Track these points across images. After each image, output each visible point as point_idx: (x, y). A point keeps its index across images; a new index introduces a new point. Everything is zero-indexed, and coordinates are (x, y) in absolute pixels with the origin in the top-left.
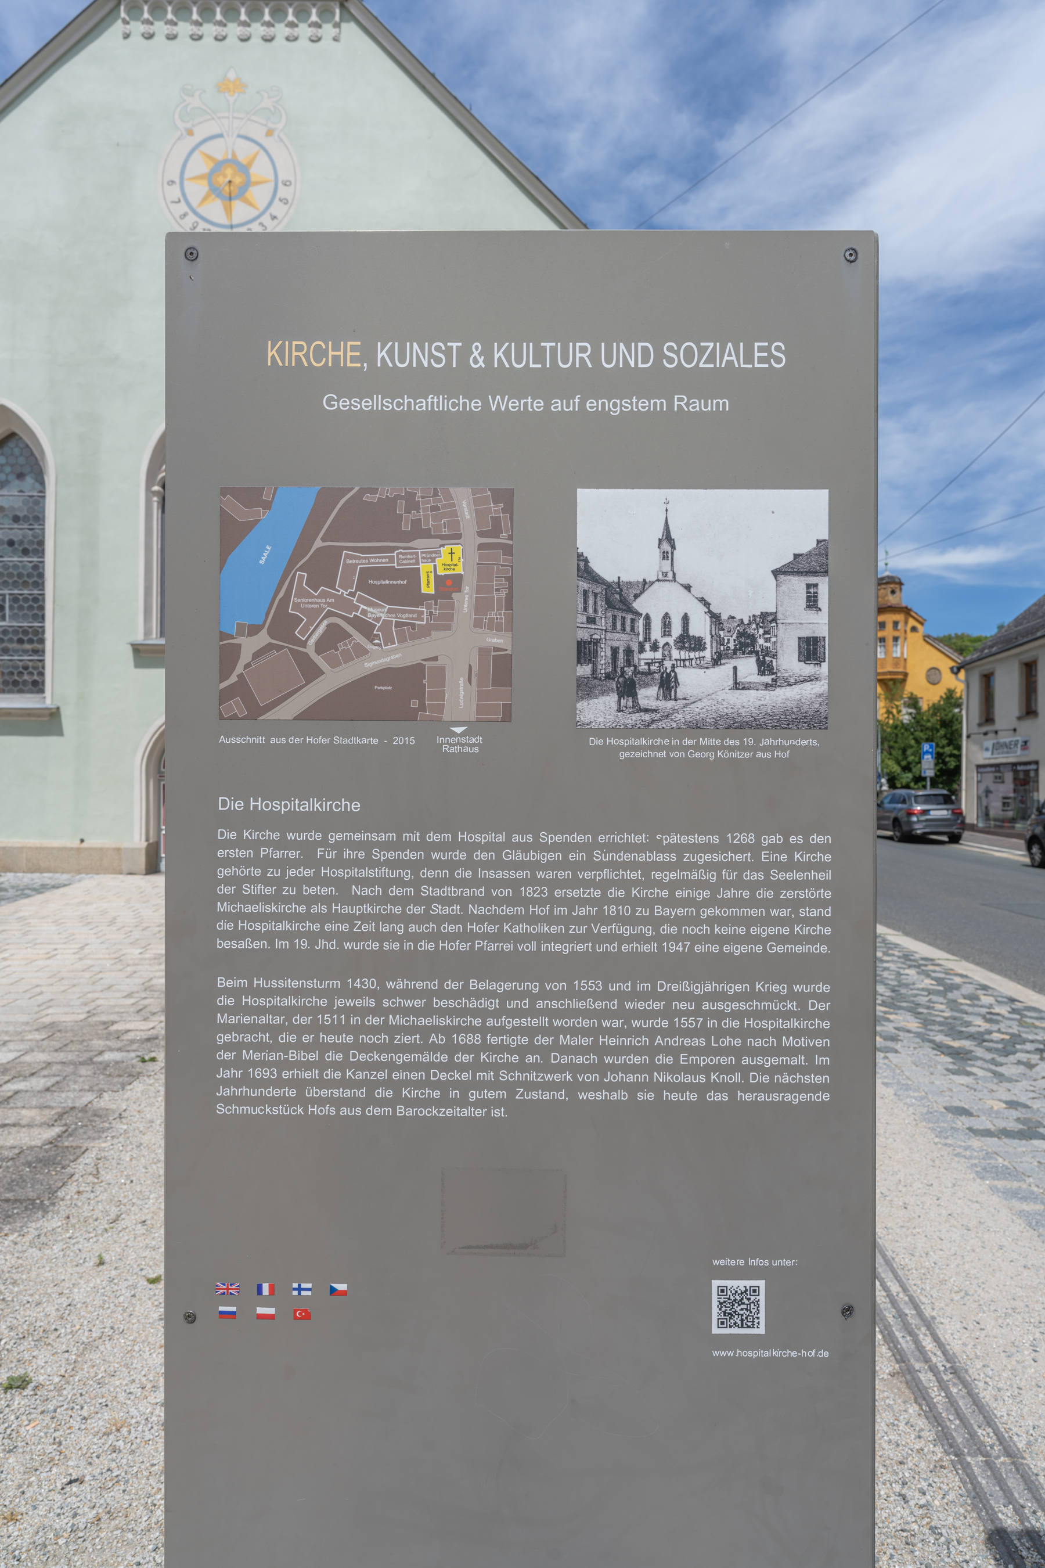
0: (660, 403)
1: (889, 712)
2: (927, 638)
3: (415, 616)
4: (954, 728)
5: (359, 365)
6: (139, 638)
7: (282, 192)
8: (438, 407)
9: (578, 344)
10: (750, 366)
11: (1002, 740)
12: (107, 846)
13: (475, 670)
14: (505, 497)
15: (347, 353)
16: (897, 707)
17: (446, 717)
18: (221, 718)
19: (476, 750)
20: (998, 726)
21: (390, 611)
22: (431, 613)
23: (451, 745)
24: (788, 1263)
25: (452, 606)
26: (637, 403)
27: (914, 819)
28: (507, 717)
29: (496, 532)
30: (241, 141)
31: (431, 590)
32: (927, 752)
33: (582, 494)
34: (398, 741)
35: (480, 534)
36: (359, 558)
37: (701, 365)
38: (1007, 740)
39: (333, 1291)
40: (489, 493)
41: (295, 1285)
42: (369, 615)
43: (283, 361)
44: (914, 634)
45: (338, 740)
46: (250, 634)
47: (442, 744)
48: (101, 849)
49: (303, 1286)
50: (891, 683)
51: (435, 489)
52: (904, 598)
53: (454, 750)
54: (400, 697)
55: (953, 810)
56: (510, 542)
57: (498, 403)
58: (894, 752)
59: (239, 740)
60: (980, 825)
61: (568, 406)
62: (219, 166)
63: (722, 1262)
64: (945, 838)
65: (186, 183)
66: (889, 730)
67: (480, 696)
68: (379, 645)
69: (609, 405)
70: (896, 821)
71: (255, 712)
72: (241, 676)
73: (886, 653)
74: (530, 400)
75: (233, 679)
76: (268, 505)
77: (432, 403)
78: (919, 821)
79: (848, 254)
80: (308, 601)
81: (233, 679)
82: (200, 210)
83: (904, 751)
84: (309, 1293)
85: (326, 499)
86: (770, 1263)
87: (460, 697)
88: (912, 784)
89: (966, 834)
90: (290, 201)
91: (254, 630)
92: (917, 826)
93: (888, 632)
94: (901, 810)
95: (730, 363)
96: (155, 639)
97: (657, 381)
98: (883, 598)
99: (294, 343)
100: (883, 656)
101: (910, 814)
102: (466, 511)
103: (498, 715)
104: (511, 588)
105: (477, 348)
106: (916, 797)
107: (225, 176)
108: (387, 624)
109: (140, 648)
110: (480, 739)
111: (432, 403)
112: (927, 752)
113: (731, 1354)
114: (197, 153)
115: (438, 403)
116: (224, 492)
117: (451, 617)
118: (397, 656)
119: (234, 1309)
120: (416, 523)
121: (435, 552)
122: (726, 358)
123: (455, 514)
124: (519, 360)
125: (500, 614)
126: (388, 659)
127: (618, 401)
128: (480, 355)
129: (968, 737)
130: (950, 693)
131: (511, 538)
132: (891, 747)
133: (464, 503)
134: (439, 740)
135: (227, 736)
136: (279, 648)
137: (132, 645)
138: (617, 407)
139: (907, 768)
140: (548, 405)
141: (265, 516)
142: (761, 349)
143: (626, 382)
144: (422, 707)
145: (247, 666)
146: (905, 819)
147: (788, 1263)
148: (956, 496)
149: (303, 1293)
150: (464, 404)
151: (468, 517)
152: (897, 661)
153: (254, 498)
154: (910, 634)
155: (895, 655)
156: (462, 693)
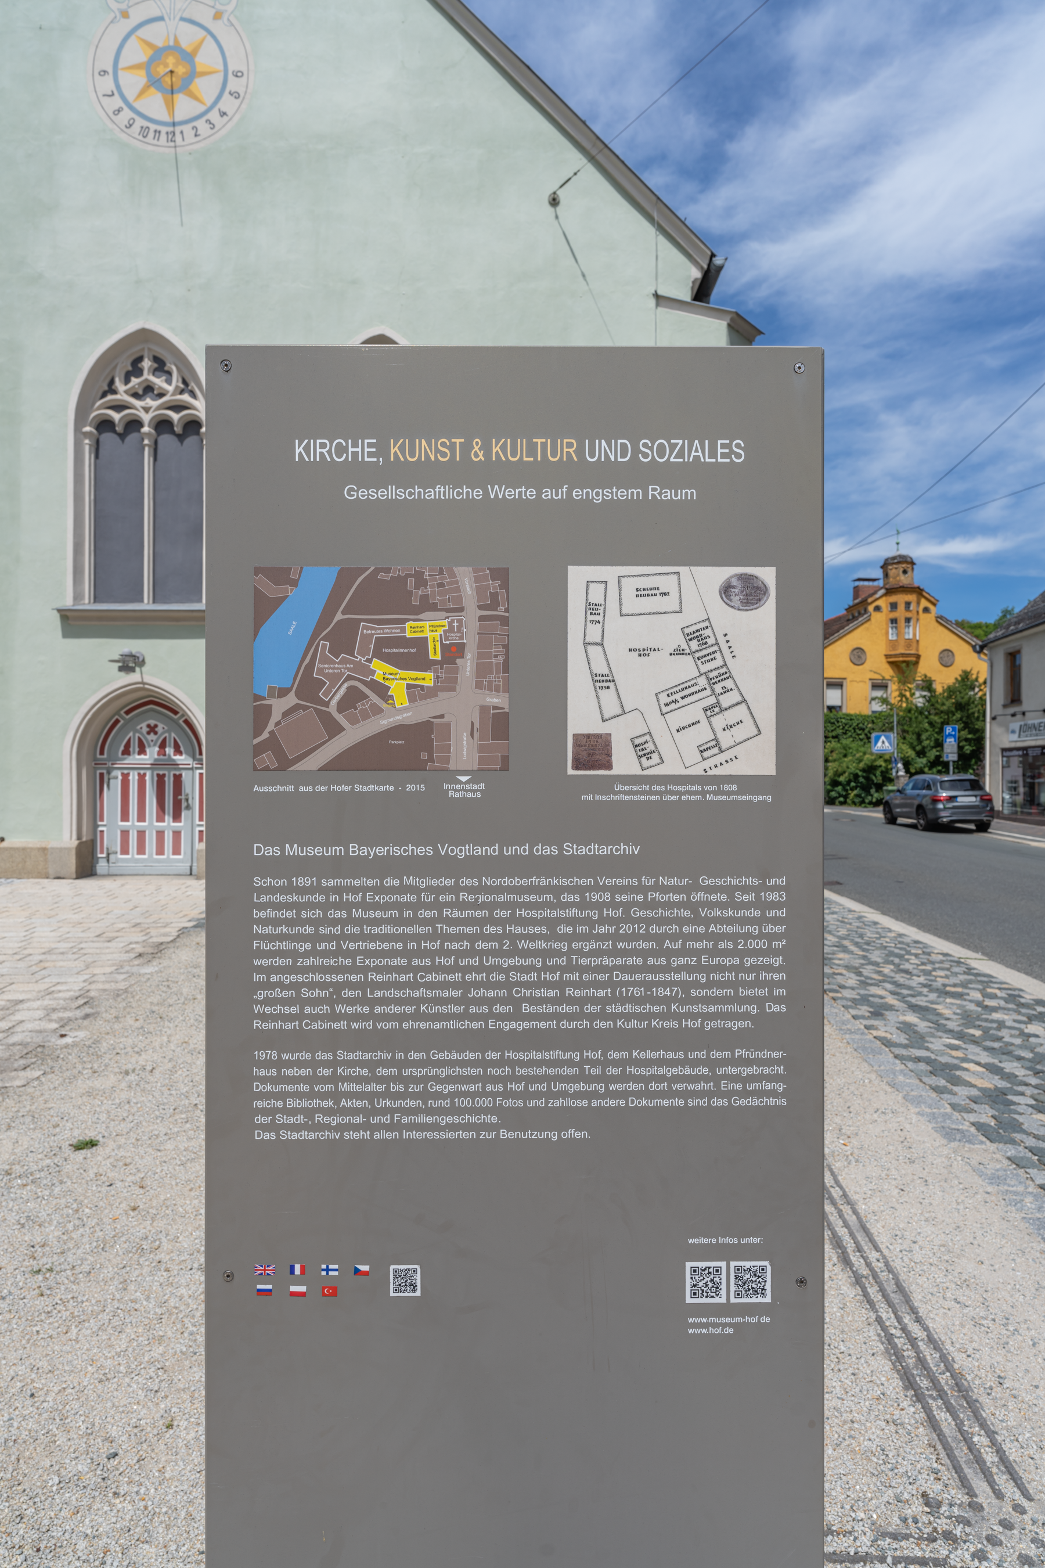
0: (636, 492)
1: (902, 695)
2: (940, 620)
4: (971, 711)
6: (68, 602)
7: (233, 84)
8: (444, 495)
11: (1030, 722)
12: (30, 846)
13: (476, 726)
14: (501, 575)
15: (364, 450)
16: (910, 689)
17: (452, 766)
19: (479, 795)
20: (1025, 706)
22: (438, 677)
23: (456, 791)
27: (940, 806)
28: (505, 767)
29: (494, 605)
30: (184, 25)
31: (438, 657)
32: (950, 735)
33: (569, 567)
34: (410, 788)
35: (480, 607)
36: (375, 629)
37: (672, 460)
38: (1036, 722)
39: (357, 1271)
41: (324, 1267)
43: (309, 458)
44: (926, 615)
45: (358, 788)
47: (448, 790)
48: (24, 849)
49: (331, 1267)
50: (904, 665)
52: (917, 578)
53: (457, 795)
54: (410, 749)
55: (981, 796)
56: (507, 614)
57: (496, 492)
60: (1006, 812)
61: (557, 495)
62: (158, 54)
63: (696, 1241)
64: (972, 827)
65: (120, 73)
66: (901, 714)
67: (482, 749)
69: (592, 494)
70: (920, 808)
71: (284, 764)
72: (272, 733)
73: (897, 635)
74: (523, 489)
75: (265, 735)
80: (331, 667)
81: (265, 735)
82: (137, 105)
83: (919, 735)
84: (336, 1273)
85: (345, 577)
87: (464, 750)
88: (926, 770)
89: (995, 822)
90: (242, 95)
91: (283, 692)
92: (943, 814)
93: (901, 613)
94: (925, 796)
95: (697, 458)
96: (87, 604)
97: (634, 473)
98: (895, 578)
100: (895, 638)
101: (935, 800)
103: (496, 766)
104: (507, 654)
105: (477, 443)
106: (942, 782)
107: (166, 65)
109: (68, 614)
112: (950, 735)
114: (133, 39)
115: (444, 492)
116: (257, 571)
117: (455, 680)
118: (409, 714)
119: (270, 1287)
122: (693, 454)
123: (458, 589)
124: (514, 455)
126: (400, 717)
129: (994, 718)
130: (966, 675)
131: (507, 610)
132: (904, 731)
133: (466, 580)
134: (446, 786)
135: (260, 785)
137: (59, 611)
138: (599, 496)
139: (921, 753)
142: (723, 446)
143: (607, 474)
144: (431, 759)
145: (278, 724)
146: (931, 807)
147: (756, 1240)
148: (957, 487)
149: (331, 1273)
152: (909, 643)
153: (282, 576)
154: (922, 615)
155: (907, 637)
156: (465, 746)
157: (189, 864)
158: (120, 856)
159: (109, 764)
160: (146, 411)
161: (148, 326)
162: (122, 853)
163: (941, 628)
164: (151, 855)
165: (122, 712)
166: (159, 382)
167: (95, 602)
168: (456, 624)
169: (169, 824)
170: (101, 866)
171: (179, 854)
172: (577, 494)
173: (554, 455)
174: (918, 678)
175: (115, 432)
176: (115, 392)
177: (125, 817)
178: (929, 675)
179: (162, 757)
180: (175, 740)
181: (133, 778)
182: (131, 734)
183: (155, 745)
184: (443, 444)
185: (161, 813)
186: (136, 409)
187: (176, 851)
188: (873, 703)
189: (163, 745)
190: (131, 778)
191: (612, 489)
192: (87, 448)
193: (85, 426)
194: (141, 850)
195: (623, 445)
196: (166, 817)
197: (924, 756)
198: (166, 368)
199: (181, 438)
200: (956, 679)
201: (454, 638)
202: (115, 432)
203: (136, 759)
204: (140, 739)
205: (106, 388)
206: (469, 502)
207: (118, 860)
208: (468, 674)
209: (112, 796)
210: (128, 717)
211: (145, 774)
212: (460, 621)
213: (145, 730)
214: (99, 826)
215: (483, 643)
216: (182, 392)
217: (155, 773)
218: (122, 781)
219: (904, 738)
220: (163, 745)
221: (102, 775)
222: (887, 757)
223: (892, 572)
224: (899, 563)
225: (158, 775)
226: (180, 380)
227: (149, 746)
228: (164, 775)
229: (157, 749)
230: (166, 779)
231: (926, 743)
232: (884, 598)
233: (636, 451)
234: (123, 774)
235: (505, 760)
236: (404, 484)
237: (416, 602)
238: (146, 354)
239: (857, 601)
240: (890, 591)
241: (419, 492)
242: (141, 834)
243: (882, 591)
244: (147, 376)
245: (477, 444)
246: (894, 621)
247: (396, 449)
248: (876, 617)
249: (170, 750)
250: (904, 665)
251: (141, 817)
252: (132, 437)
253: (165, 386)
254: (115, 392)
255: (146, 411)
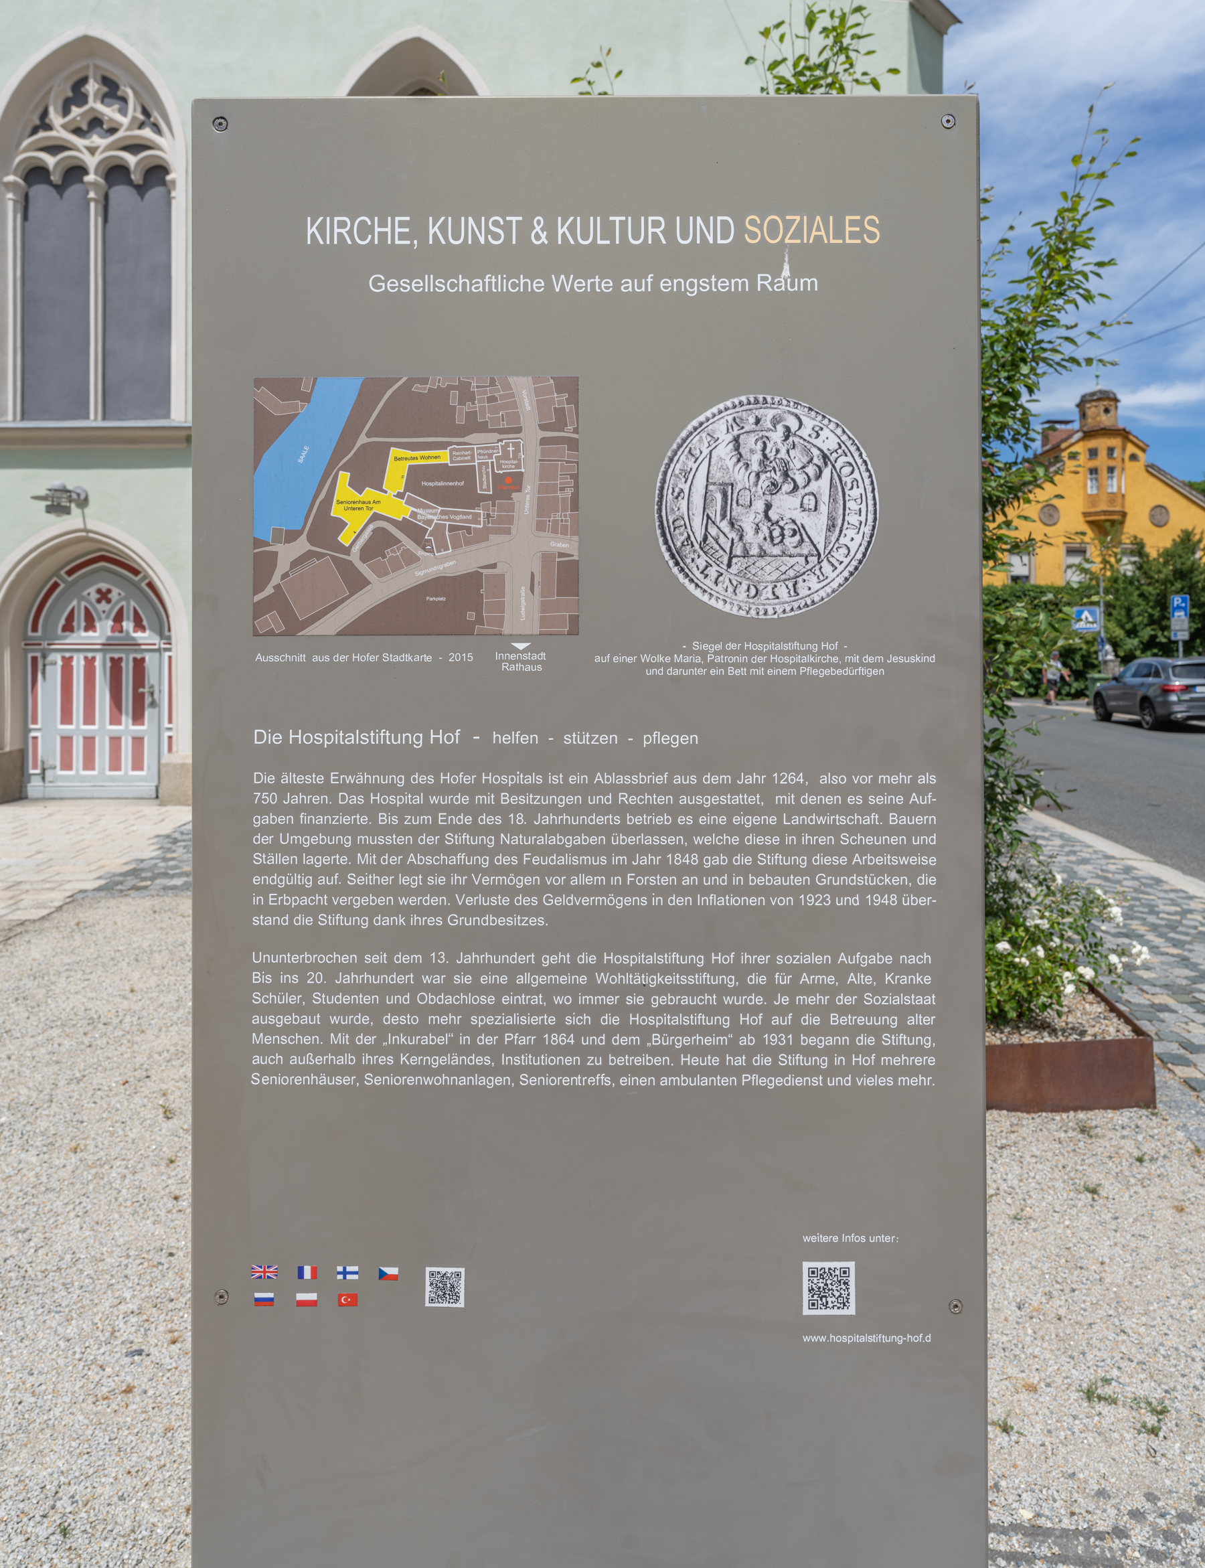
1: (1105, 562)
3: (470, 517)
4: (1194, 580)
5: (408, 242)
8: (496, 288)
9: (650, 219)
10: (841, 241)
14: (569, 386)
15: (395, 230)
16: (1116, 554)
17: (506, 630)
18: (256, 634)
19: (539, 668)
21: (442, 513)
22: (489, 516)
23: (511, 662)
24: (887, 1239)
25: (511, 508)
26: (716, 283)
27: (1174, 698)
28: (574, 631)
29: (560, 424)
32: (1179, 608)
34: (454, 657)
35: (543, 427)
37: (787, 241)
39: (382, 1275)
40: (552, 382)
41: (340, 1269)
42: (419, 517)
44: (1134, 464)
46: (288, 541)
47: (502, 661)
49: (349, 1269)
51: (492, 380)
53: (513, 668)
56: (576, 436)
58: (1115, 613)
59: (277, 659)
61: (640, 287)
63: (813, 1239)
67: (544, 607)
68: (431, 551)
71: (293, 627)
72: (277, 587)
73: (1098, 488)
74: (597, 280)
75: (269, 590)
76: (306, 398)
77: (490, 283)
78: (1180, 701)
79: (944, 120)
81: (269, 590)
83: (1129, 610)
84: (356, 1277)
85: (370, 392)
86: (867, 1239)
87: (522, 609)
91: (291, 536)
92: (1176, 708)
93: (1102, 461)
94: (1151, 685)
95: (818, 239)
98: (1094, 418)
99: (336, 219)
100: (1095, 492)
101: (1166, 691)
102: (527, 402)
103: (565, 629)
104: (576, 487)
106: (1174, 667)
108: (439, 529)
110: (543, 654)
111: (490, 283)
112: (1179, 608)
113: (823, 1339)
115: (496, 283)
116: (258, 383)
117: (510, 520)
119: (271, 1295)
120: (472, 416)
121: (493, 448)
122: (814, 233)
123: (514, 405)
124: (585, 236)
125: (565, 516)
126: (441, 567)
127: (696, 281)
128: (542, 230)
131: (576, 431)
134: (497, 656)
135: (265, 654)
136: (320, 556)
138: (694, 287)
139: (1132, 633)
140: (617, 285)
141: (304, 410)
142: (852, 223)
143: (702, 260)
144: (480, 620)
145: (285, 576)
146: (1160, 699)
147: (887, 1239)
149: (349, 1277)
150: (526, 284)
151: (529, 408)
152: (1112, 498)
153: (292, 389)
155: (1110, 490)
157: (155, 783)
158: (60, 772)
159: (45, 645)
160: (93, 152)
161: (92, 32)
162: (62, 769)
163: (1152, 480)
164: (102, 771)
165: (62, 572)
166: (110, 112)
167: (23, 419)
168: (511, 449)
169: (127, 728)
170: (34, 787)
171: (142, 769)
172: (665, 285)
173: (636, 237)
174: (1126, 540)
175: (50, 183)
176: (49, 127)
177: (67, 717)
178: (1140, 536)
179: (117, 634)
180: (135, 611)
181: (78, 663)
182: (74, 603)
183: (107, 618)
184: (496, 224)
185: (116, 712)
186: (79, 150)
187: (137, 764)
188: (1069, 572)
189: (118, 618)
190: (74, 663)
191: (710, 278)
192: (10, 205)
193: (7, 175)
194: (89, 763)
195: (724, 223)
196: (124, 718)
197: (1136, 636)
198: (119, 93)
199: (141, 189)
200: (1174, 540)
201: (509, 467)
202: (50, 183)
203: (81, 636)
204: (86, 609)
205: (37, 122)
206: (528, 295)
207: (56, 778)
208: (527, 511)
209: (48, 689)
210: (70, 579)
211: (94, 658)
212: (516, 445)
213: (94, 596)
214: (30, 730)
215: (546, 472)
216: (141, 126)
217: (108, 656)
218: (63, 667)
219: (1110, 614)
220: (118, 618)
221: (35, 659)
222: (1089, 638)
223: (1091, 411)
224: (1099, 400)
225: (112, 659)
226: (139, 109)
227: (100, 619)
228: (120, 659)
229: (110, 623)
230: (123, 664)
231: (1138, 620)
232: (1081, 443)
233: (741, 229)
234: (63, 658)
235: (574, 621)
236: (445, 273)
237: (460, 420)
238: (91, 73)
239: (1047, 448)
240: (1088, 435)
241: (464, 283)
242: (89, 741)
243: (1079, 435)
244: (94, 104)
245: (538, 224)
246: (1094, 471)
247: (436, 228)
248: (1070, 465)
249: (128, 625)
250: (1106, 525)
251: (89, 718)
252: (73, 190)
253: (118, 117)
254: (49, 127)
255: (93, 152)
